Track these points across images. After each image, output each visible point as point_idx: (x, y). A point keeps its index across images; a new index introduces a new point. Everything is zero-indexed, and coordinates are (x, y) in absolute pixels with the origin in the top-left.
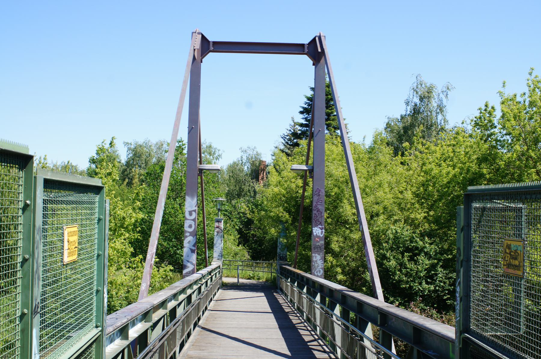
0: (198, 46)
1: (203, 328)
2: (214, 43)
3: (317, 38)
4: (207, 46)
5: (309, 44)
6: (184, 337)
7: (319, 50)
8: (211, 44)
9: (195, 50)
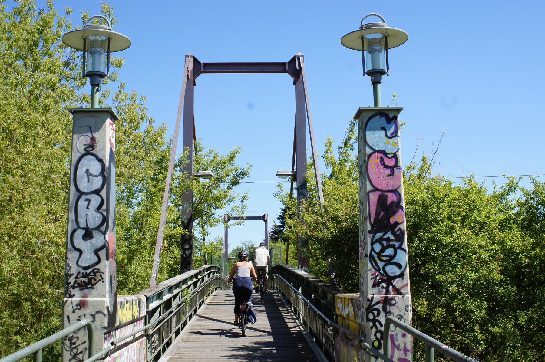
0: (191, 67)
2: (206, 64)
3: (296, 59)
4: (199, 68)
5: (289, 62)
7: (298, 68)
8: (202, 65)
9: (188, 71)
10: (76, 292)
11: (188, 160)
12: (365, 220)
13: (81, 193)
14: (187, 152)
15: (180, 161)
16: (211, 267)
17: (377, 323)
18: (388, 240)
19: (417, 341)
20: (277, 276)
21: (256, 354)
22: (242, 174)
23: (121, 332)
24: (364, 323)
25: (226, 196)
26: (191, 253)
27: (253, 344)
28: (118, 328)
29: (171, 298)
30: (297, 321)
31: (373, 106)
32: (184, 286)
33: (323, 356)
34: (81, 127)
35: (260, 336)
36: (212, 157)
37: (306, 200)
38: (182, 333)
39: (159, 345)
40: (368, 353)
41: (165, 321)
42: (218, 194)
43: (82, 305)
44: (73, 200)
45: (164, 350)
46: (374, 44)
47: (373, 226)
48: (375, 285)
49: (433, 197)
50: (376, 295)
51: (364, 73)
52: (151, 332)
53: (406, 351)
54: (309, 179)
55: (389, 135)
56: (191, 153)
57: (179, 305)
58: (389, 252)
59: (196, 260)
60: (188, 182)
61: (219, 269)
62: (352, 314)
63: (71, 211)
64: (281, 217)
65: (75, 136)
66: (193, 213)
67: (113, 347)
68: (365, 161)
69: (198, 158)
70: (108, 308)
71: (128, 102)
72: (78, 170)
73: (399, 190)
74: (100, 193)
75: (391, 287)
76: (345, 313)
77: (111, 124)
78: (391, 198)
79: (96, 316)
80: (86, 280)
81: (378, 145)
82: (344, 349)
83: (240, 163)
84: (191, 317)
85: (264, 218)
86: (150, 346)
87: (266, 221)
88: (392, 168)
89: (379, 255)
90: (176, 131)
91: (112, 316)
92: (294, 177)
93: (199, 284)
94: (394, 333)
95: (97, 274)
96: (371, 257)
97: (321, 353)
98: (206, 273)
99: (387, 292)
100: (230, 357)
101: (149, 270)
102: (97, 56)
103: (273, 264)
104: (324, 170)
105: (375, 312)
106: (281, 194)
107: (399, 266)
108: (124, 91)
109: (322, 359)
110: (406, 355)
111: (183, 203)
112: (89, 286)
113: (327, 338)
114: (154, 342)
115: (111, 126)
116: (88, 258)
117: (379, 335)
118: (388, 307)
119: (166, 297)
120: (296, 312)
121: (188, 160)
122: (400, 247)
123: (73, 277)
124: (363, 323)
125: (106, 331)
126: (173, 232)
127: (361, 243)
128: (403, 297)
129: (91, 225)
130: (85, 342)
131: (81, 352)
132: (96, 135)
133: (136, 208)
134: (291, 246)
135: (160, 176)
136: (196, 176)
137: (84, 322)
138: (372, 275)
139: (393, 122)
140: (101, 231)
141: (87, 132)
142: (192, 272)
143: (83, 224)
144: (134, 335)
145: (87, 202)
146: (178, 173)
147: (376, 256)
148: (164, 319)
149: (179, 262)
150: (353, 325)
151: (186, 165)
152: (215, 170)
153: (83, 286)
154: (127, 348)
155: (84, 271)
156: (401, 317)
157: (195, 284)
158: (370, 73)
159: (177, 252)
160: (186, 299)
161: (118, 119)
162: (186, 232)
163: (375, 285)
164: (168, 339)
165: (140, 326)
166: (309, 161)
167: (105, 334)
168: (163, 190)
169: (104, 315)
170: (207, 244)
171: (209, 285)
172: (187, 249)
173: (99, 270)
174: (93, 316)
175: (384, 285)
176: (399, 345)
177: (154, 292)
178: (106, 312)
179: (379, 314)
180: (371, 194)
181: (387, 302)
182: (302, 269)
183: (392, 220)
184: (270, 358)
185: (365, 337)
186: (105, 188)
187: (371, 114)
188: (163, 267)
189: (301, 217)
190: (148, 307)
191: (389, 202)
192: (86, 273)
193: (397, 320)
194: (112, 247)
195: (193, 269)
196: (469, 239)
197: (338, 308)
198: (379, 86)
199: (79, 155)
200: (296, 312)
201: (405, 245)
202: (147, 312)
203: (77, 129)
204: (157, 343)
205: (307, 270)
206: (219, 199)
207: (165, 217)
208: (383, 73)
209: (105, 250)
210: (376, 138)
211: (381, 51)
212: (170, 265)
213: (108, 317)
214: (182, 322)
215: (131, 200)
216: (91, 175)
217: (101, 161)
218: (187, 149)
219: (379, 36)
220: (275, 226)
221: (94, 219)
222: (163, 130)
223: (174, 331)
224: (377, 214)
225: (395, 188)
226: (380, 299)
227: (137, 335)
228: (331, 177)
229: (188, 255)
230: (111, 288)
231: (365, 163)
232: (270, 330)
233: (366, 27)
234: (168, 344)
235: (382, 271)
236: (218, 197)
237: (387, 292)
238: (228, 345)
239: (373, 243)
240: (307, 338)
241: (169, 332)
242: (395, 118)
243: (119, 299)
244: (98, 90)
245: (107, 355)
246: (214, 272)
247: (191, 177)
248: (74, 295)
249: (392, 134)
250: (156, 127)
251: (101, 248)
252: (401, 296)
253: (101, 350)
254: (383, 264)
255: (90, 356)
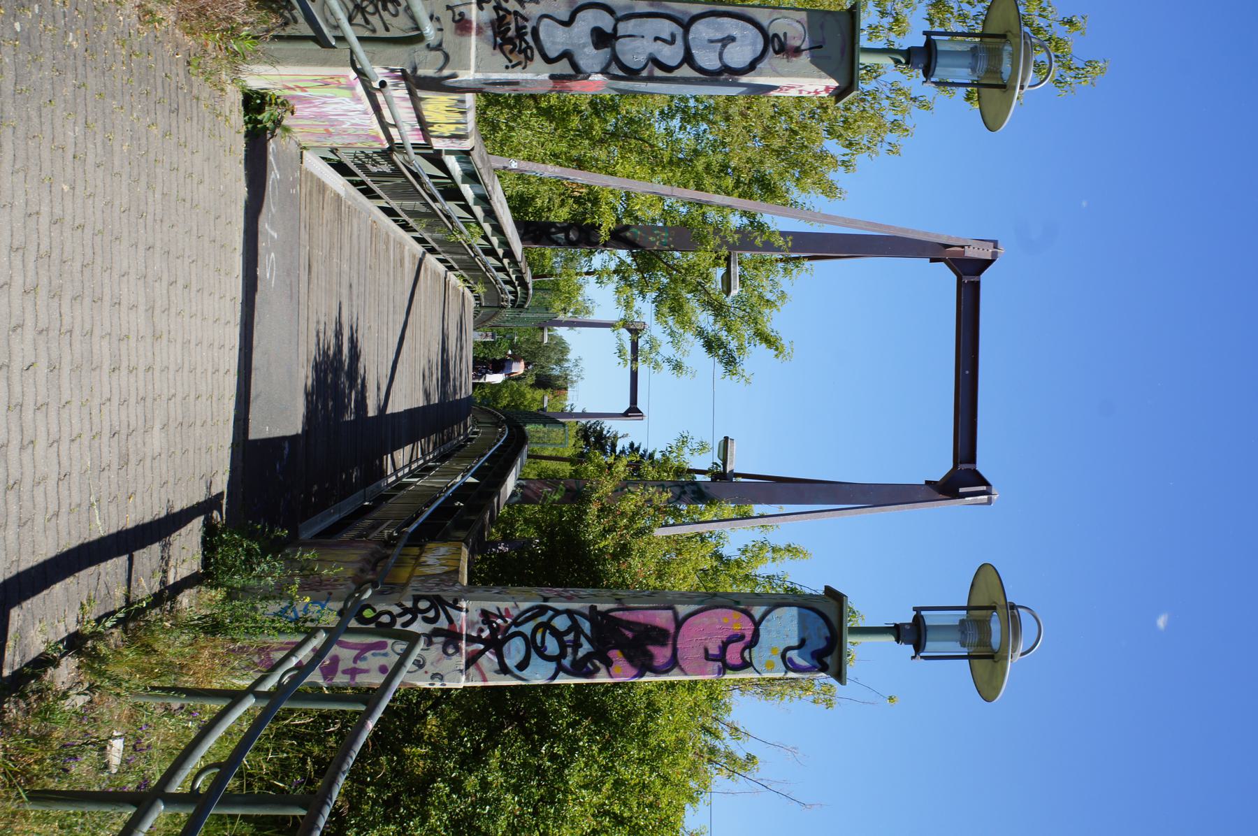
0: (971, 253)
1: (421, 261)
2: (976, 286)
4: (969, 271)
6: (405, 217)
7: (962, 490)
10: (488, 13)
11: (764, 243)
12: (619, 600)
13: (686, 25)
14: (781, 242)
15: (761, 227)
16: (527, 289)
17: (409, 616)
18: (577, 645)
19: (369, 697)
20: (502, 434)
21: (343, 378)
22: (730, 362)
23: (404, 99)
24: (410, 592)
25: (683, 324)
26: (559, 244)
27: (362, 372)
28: (412, 94)
29: (463, 199)
30: (407, 470)
31: (849, 625)
32: (487, 227)
33: (336, 518)
34: (822, 26)
35: (379, 389)
36: (768, 296)
37: (668, 501)
38: (387, 221)
39: (369, 173)
40: (351, 596)
41: (418, 187)
42: (686, 307)
43: (462, 24)
44: (673, 9)
45: (355, 184)
46: (981, 632)
47: (605, 614)
48: (485, 614)
49: (661, 751)
50: (467, 615)
51: (918, 610)
52: (397, 158)
53: (353, 672)
54: (715, 510)
55: (789, 654)
56: (779, 249)
57: (448, 217)
58: (552, 646)
59: (543, 255)
60: (713, 242)
61: (521, 306)
62: (428, 571)
63: (652, 5)
64: (633, 449)
65: (803, 15)
66: (650, 252)
67: (376, 85)
68: (738, 603)
69: (768, 266)
70: (454, 76)
71: (890, 116)
72: (735, 20)
73: (676, 670)
74: (685, 65)
75: (482, 647)
76: (429, 558)
77: (827, 89)
78: (661, 654)
79: (439, 53)
80: (512, 33)
81: (769, 632)
82: (356, 555)
83: (755, 357)
84: (421, 241)
85: (633, 411)
86: (367, 156)
87: (626, 415)
88: (721, 657)
89: (547, 626)
90: (828, 219)
91: (437, 85)
92: (721, 476)
93: (491, 261)
94: (388, 649)
95: (522, 56)
96: (542, 610)
97: (343, 515)
98: (514, 277)
99: (471, 640)
100: (339, 323)
101: (525, 153)
102: (968, 61)
103: (529, 428)
104: (736, 539)
105: (431, 614)
106: (686, 450)
107: (523, 666)
108: (914, 108)
109: (331, 515)
110: (345, 672)
111: (669, 229)
112: (499, 40)
113: (373, 527)
114: (376, 163)
115: (821, 88)
116: (555, 38)
117: (385, 619)
118: (441, 639)
119: (468, 191)
120: (424, 470)
121: (764, 243)
122: (560, 669)
123: (518, 8)
124: (409, 589)
125: (409, 71)
126: (604, 208)
127: (571, 591)
128: (461, 671)
129: (622, 46)
130: (387, 30)
131: (367, 21)
132: (805, 59)
133: (659, 128)
134: (567, 468)
135: (729, 182)
136: (728, 259)
137: (429, 30)
138: (507, 610)
139: (816, 663)
140: (608, 65)
141: (811, 40)
142: (517, 247)
143: (623, 28)
144: (395, 126)
145: (669, 38)
146: (735, 221)
147: (544, 619)
148: (421, 184)
149: (541, 217)
150: (404, 574)
151: (753, 236)
152: (740, 300)
153: (499, 27)
154: (370, 110)
155: (529, 30)
156: (420, 664)
157: (491, 252)
158: (918, 620)
159: (562, 214)
160: (461, 232)
161: (837, 101)
162: (604, 234)
163: (485, 614)
164: (379, 192)
165: (414, 137)
166: (757, 509)
167: (403, 71)
168: (699, 187)
169: (441, 69)
170: (580, 279)
171: (487, 282)
172: (567, 236)
173: (531, 59)
174: (439, 47)
175: (486, 634)
176: (365, 659)
177: (480, 165)
178: (446, 72)
179: (426, 620)
180: (670, 613)
181: (452, 638)
182: (518, 486)
183: (616, 655)
184: (334, 406)
185: (382, 593)
186: (697, 75)
187: (834, 619)
188: (529, 183)
189: (632, 489)
190: (449, 152)
191: (654, 649)
192: (526, 34)
193: (414, 656)
194: (576, 86)
195: (524, 249)
196: (573, 822)
197: (437, 548)
198: (891, 639)
199: (765, 23)
200: (424, 470)
201: (562, 680)
202: (439, 152)
203: (818, 19)
204: (374, 169)
205: (515, 499)
206: (677, 308)
207: (636, 189)
208: (919, 647)
209: (571, 72)
210: (783, 628)
211: (963, 645)
212: (533, 199)
213: (436, 75)
214: (411, 222)
215: (678, 116)
216: (724, 46)
217: (752, 67)
218: (787, 242)
219: (996, 640)
220: (615, 437)
221: (634, 52)
222: (830, 190)
223: (394, 204)
224: (629, 625)
225: (681, 662)
226: (458, 624)
227: (393, 131)
228: (718, 557)
229: (554, 236)
230: (495, 83)
231: (732, 604)
232: (389, 411)
233: (1013, 616)
234: (368, 193)
235: (513, 629)
236: (681, 307)
237: (471, 640)
238: (361, 318)
239: (570, 613)
240: (372, 487)
241: (393, 196)
242: (824, 668)
243: (470, 98)
244: (897, 62)
245: (361, 74)
246: (515, 293)
247: (725, 248)
248: (481, 8)
249: (791, 660)
250: (836, 176)
251: (575, 66)
252: (463, 667)
253: (372, 61)
254: (528, 633)
255: (360, 39)
